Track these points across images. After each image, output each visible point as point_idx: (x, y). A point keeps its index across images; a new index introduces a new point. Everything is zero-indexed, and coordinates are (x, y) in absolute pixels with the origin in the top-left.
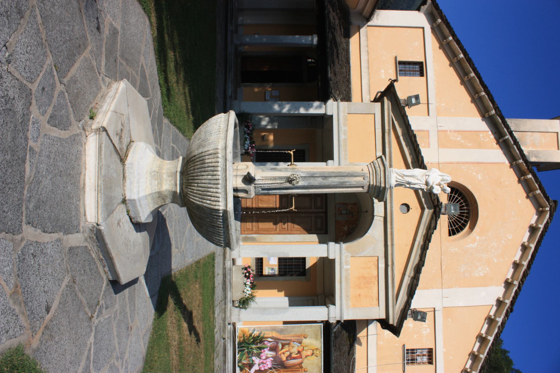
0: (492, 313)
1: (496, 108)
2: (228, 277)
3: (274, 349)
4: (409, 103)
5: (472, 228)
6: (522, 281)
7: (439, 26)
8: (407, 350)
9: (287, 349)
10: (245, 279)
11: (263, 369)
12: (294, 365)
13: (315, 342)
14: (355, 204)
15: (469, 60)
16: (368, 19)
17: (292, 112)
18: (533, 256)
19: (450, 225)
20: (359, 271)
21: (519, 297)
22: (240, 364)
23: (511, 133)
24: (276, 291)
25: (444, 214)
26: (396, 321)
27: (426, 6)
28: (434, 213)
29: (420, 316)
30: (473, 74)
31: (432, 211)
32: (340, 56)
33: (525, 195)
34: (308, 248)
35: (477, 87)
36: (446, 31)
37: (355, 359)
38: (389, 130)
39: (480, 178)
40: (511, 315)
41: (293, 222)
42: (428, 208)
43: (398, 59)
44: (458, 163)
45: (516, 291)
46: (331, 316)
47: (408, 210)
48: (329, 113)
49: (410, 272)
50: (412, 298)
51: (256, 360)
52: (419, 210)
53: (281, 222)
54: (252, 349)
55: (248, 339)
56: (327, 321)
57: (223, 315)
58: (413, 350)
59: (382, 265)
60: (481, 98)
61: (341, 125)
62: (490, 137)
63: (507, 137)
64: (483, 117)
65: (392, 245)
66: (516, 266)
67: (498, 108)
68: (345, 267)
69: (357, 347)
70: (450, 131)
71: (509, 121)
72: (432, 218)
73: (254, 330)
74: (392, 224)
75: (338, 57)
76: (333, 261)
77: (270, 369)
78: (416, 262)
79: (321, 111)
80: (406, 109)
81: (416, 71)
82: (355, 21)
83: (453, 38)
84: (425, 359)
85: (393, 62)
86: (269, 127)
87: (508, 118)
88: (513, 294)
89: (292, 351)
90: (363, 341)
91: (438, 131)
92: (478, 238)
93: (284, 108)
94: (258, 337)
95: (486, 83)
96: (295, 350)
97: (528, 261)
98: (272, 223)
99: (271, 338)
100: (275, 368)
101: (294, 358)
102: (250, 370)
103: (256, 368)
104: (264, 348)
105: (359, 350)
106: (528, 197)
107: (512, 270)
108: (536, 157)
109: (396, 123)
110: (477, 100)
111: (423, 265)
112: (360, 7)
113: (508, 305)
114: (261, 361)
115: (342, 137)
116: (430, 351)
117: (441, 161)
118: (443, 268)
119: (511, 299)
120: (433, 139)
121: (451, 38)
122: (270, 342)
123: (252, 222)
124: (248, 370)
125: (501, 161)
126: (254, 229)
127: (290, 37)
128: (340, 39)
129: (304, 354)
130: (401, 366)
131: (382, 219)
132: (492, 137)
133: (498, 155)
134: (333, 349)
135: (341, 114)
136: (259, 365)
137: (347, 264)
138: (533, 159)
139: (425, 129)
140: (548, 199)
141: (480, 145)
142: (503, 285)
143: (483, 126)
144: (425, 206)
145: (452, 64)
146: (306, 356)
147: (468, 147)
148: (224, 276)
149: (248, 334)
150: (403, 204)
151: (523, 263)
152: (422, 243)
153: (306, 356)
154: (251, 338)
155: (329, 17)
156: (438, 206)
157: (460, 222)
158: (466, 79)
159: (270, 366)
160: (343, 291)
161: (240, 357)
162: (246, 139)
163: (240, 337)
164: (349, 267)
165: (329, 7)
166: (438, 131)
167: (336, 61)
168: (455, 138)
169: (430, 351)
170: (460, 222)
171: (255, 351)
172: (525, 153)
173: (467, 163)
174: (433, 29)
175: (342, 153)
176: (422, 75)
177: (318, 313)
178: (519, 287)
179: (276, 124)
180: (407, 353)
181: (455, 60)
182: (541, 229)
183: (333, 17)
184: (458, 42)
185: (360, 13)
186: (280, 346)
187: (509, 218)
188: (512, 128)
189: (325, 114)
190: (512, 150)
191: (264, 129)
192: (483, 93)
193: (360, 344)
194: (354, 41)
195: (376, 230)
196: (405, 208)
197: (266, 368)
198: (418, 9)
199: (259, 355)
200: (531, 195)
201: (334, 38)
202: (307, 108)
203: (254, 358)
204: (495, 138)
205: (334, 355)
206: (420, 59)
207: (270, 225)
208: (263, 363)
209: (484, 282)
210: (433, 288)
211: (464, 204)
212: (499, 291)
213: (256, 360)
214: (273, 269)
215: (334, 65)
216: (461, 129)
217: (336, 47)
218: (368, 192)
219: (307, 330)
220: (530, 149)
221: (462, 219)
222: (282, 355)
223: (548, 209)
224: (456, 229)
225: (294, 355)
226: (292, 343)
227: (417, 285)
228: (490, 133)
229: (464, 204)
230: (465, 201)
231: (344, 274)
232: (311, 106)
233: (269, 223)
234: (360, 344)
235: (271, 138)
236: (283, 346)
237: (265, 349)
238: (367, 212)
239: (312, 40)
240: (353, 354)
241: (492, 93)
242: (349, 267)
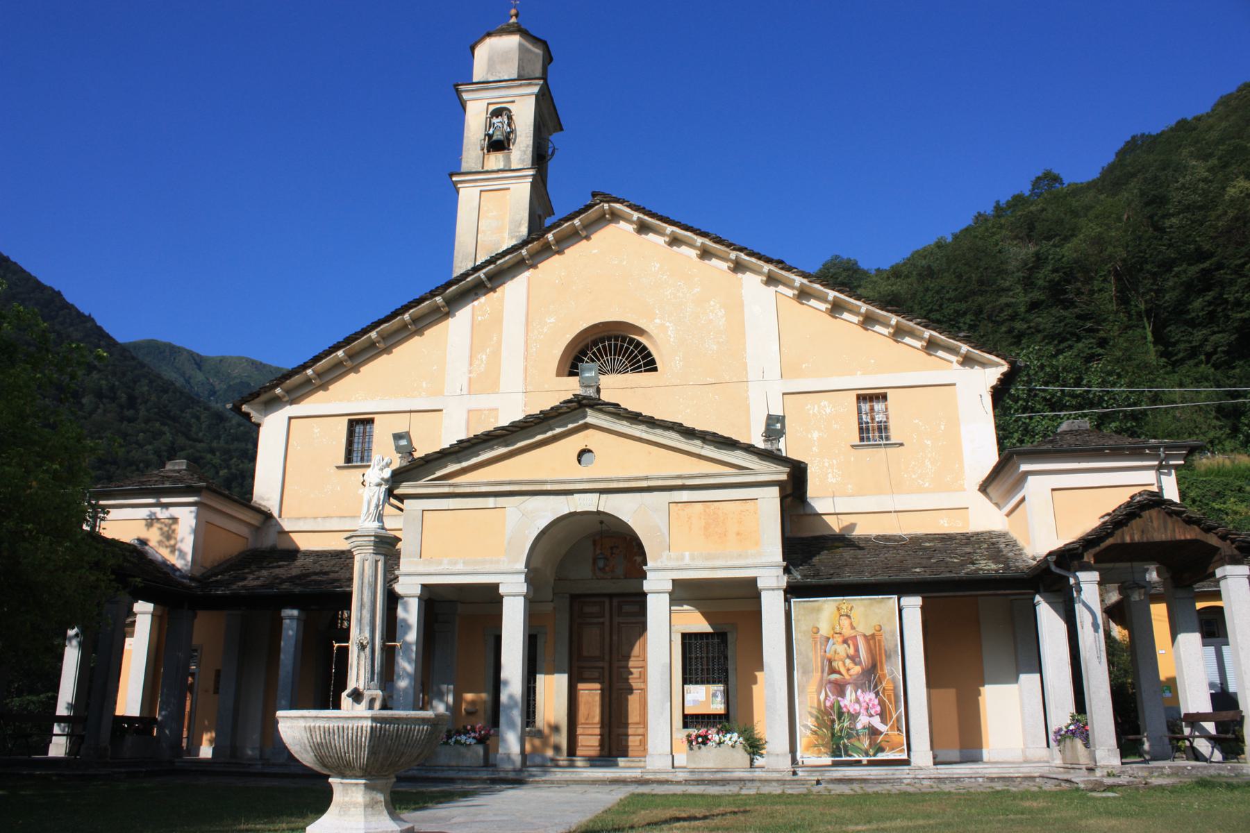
0: (790, 293)
1: (432, 294)
2: (707, 776)
3: (840, 689)
4: (408, 451)
5: (641, 332)
6: (729, 245)
7: (288, 392)
8: (862, 439)
9: (840, 663)
10: (710, 743)
11: (878, 709)
12: (871, 652)
13: (824, 613)
14: (595, 543)
15: (349, 340)
16: (268, 516)
17: (414, 656)
18: (687, 228)
19: (637, 369)
20: (701, 536)
21: (756, 250)
22: (871, 752)
23: (476, 269)
24: (756, 689)
25: (598, 391)
26: (781, 468)
27: (253, 414)
28: (591, 407)
29: (775, 427)
30: (373, 334)
31: (589, 411)
32: (326, 569)
33: (584, 242)
34: (665, 629)
35: (395, 327)
36: (297, 379)
37: (877, 537)
38: (450, 485)
39: (552, 320)
40: (789, 262)
41: (628, 657)
42: (585, 417)
43: (342, 463)
44: (526, 359)
45: (747, 255)
46: (775, 585)
47: (590, 451)
48: (418, 591)
49: (695, 446)
50: (738, 442)
51: (863, 721)
52: (590, 431)
53: (628, 679)
54: (841, 730)
55: (823, 737)
56: (786, 592)
57: (774, 784)
58: (861, 429)
59: (685, 495)
60: (415, 320)
61: (439, 569)
62: (483, 303)
63: (483, 276)
64: (447, 315)
65: (647, 479)
66: (705, 254)
67: (431, 292)
68: (687, 561)
69: (858, 532)
70: (470, 372)
71: (457, 272)
72: (601, 411)
73: (806, 726)
74: (612, 480)
75: (326, 573)
76: (675, 582)
77: (877, 694)
78: (676, 436)
79: (414, 605)
80: (417, 455)
81: (364, 432)
82: (269, 540)
83: (310, 367)
84: (879, 406)
85: (346, 472)
86: (450, 699)
87: (451, 271)
88: (753, 260)
89: (843, 654)
90: (846, 521)
91: (469, 393)
92: (658, 321)
93: (404, 670)
94: (817, 718)
95: (388, 313)
96: (842, 649)
97: (695, 237)
98: (630, 697)
99: (819, 693)
100: (876, 686)
101: (857, 650)
102: (881, 733)
103: (876, 722)
104: (840, 707)
105: (865, 528)
106: (588, 238)
107: (714, 261)
108: (520, 225)
109: (438, 474)
110: (419, 326)
111: (681, 425)
112: (244, 531)
113: (772, 267)
114: (863, 711)
115: (460, 567)
116: (862, 398)
117: (522, 389)
118: (710, 380)
119: (761, 263)
120: (483, 402)
121: (309, 372)
122: (827, 695)
123: (627, 735)
124: (881, 737)
125: (526, 284)
126: (640, 731)
127: (282, 656)
128: (296, 568)
129: (847, 632)
130: (890, 450)
131: (604, 497)
132: (483, 299)
133: (515, 290)
134: (836, 580)
135: (421, 569)
136: (871, 716)
137: (683, 559)
138: (524, 231)
139: (465, 416)
140: (588, 207)
141: (497, 320)
142: (740, 275)
143: (464, 315)
144: (581, 422)
145: (355, 369)
146: (853, 628)
147: (499, 342)
148: (699, 782)
149: (813, 738)
150: (579, 461)
151: (698, 244)
152: (643, 427)
153: (853, 628)
154: (820, 732)
155: (253, 588)
156: (579, 402)
157: (632, 352)
158: (381, 345)
159: (872, 695)
160: (730, 563)
161: (858, 753)
162: (457, 742)
163: (820, 751)
164: (687, 554)
165: (234, 587)
166: (469, 393)
167: (332, 576)
168: (479, 366)
169: (862, 398)
170: (632, 352)
171: (846, 724)
172: (514, 242)
173: (526, 342)
174: (292, 402)
175: (487, 568)
176: (371, 421)
177: (772, 606)
178: (741, 250)
179: (444, 687)
180: (868, 439)
181: (349, 364)
182: (641, 216)
183: (254, 580)
184: (317, 359)
185: (257, 530)
186: (834, 676)
187: (623, 269)
188: (470, 266)
189: (420, 598)
190: (506, 266)
191: (454, 709)
192: (406, 316)
193: (852, 526)
194: (305, 543)
195: (623, 508)
196: (585, 457)
197: (876, 702)
198: (258, 425)
199: (854, 717)
200: (584, 234)
201: (291, 580)
202: (407, 627)
203: (859, 726)
204: (485, 294)
205: (848, 577)
206: (343, 424)
207: (633, 701)
208: (867, 709)
209: (735, 308)
210: (747, 398)
211: (590, 354)
212: (751, 283)
213: (863, 721)
214: (714, 695)
215: (338, 580)
216: (467, 354)
217: (308, 575)
218: (385, 555)
219: (804, 628)
220: (506, 235)
221: (627, 349)
222: (852, 672)
223: (606, 206)
224: (643, 358)
225: (851, 651)
226: (828, 655)
227: (714, 434)
228: (476, 303)
229: (590, 354)
230: (595, 343)
231: (699, 563)
232: (404, 621)
233: (630, 703)
234: (852, 526)
235: (469, 696)
236: (833, 671)
237: (842, 704)
238: (601, 522)
239: (291, 618)
240: (867, 539)
241: (405, 302)
242: (687, 554)
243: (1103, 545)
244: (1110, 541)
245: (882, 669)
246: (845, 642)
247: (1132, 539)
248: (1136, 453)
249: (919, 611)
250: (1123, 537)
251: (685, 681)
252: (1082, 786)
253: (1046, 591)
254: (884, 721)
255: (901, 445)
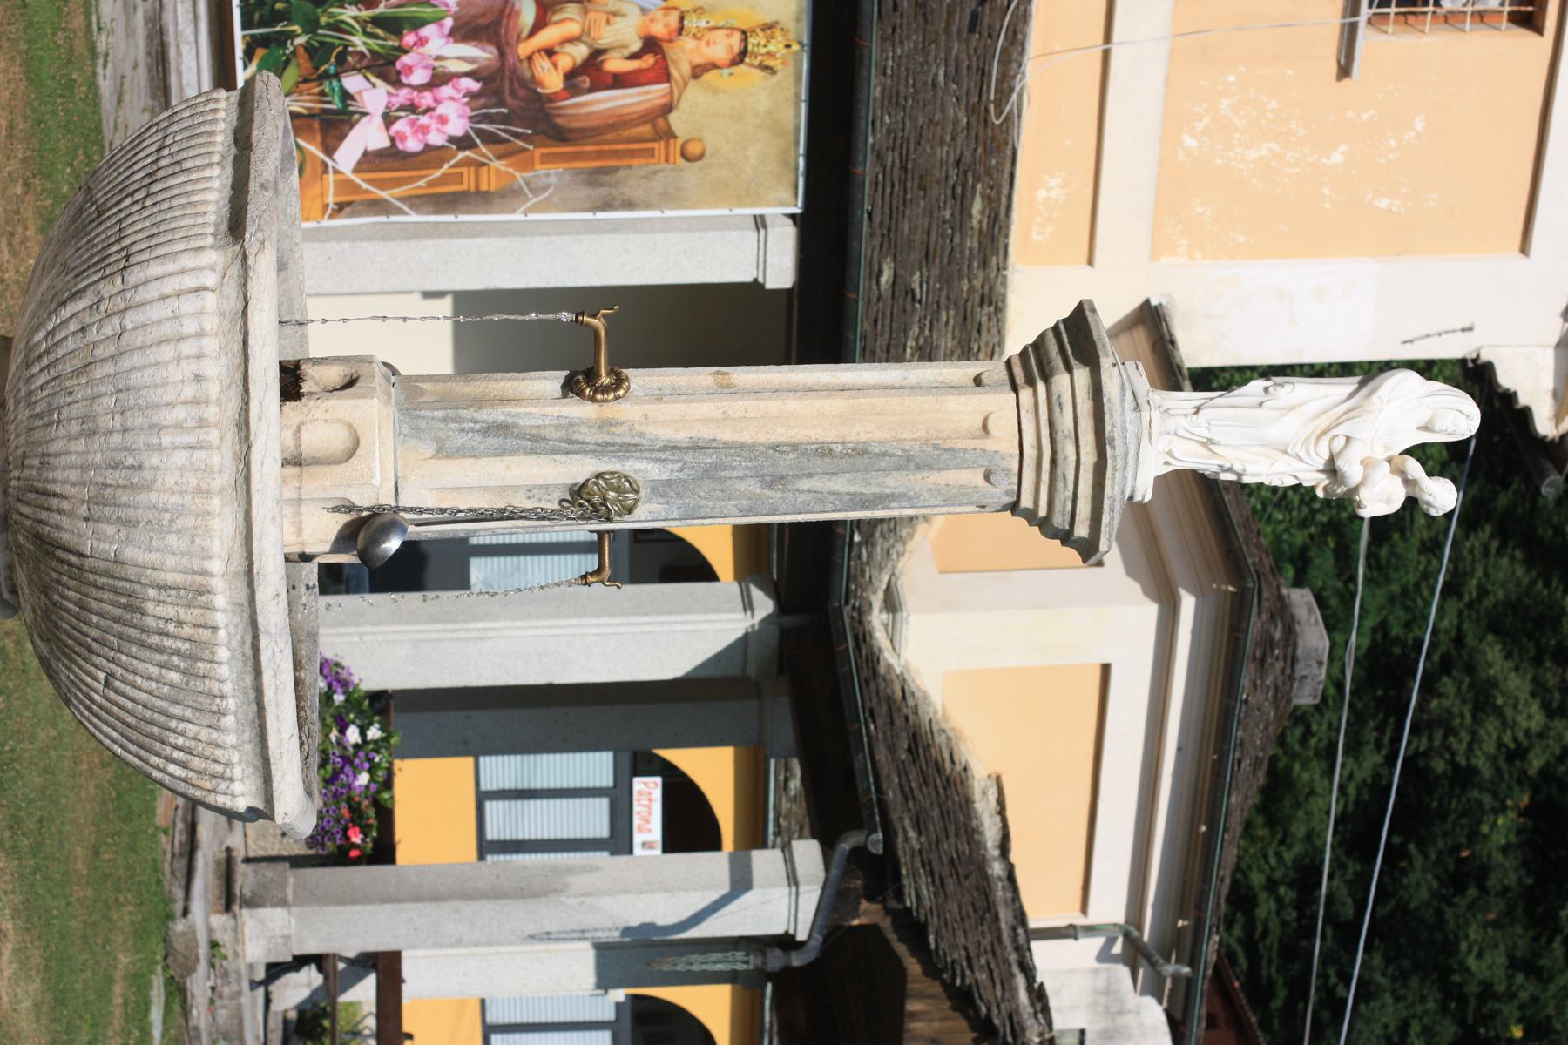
9: (573, 28)
11: (412, 145)
51: (372, 95)
54: (337, 26)
77: (463, 142)
89: (606, 36)
100: (490, 139)
101: (620, 81)
102: (330, 150)
104: (417, 23)
114: (403, 95)
129: (684, 54)
136: (388, 120)
146: (698, 71)
153: (698, 71)
159: (458, 127)
197: (436, 139)
199: (385, 67)
203: (353, 82)
208: (411, 108)
222: (542, 66)
225: (615, 64)
237: (428, 31)
243: (901, 949)
244: (913, 967)
245: (546, 159)
246: (651, 45)
247: (914, 1016)
248: (1187, 888)
249: (744, 275)
250: (921, 996)
251: (466, 302)
252: (179, 926)
253: (784, 633)
254: (370, 161)
255: (1344, 71)
